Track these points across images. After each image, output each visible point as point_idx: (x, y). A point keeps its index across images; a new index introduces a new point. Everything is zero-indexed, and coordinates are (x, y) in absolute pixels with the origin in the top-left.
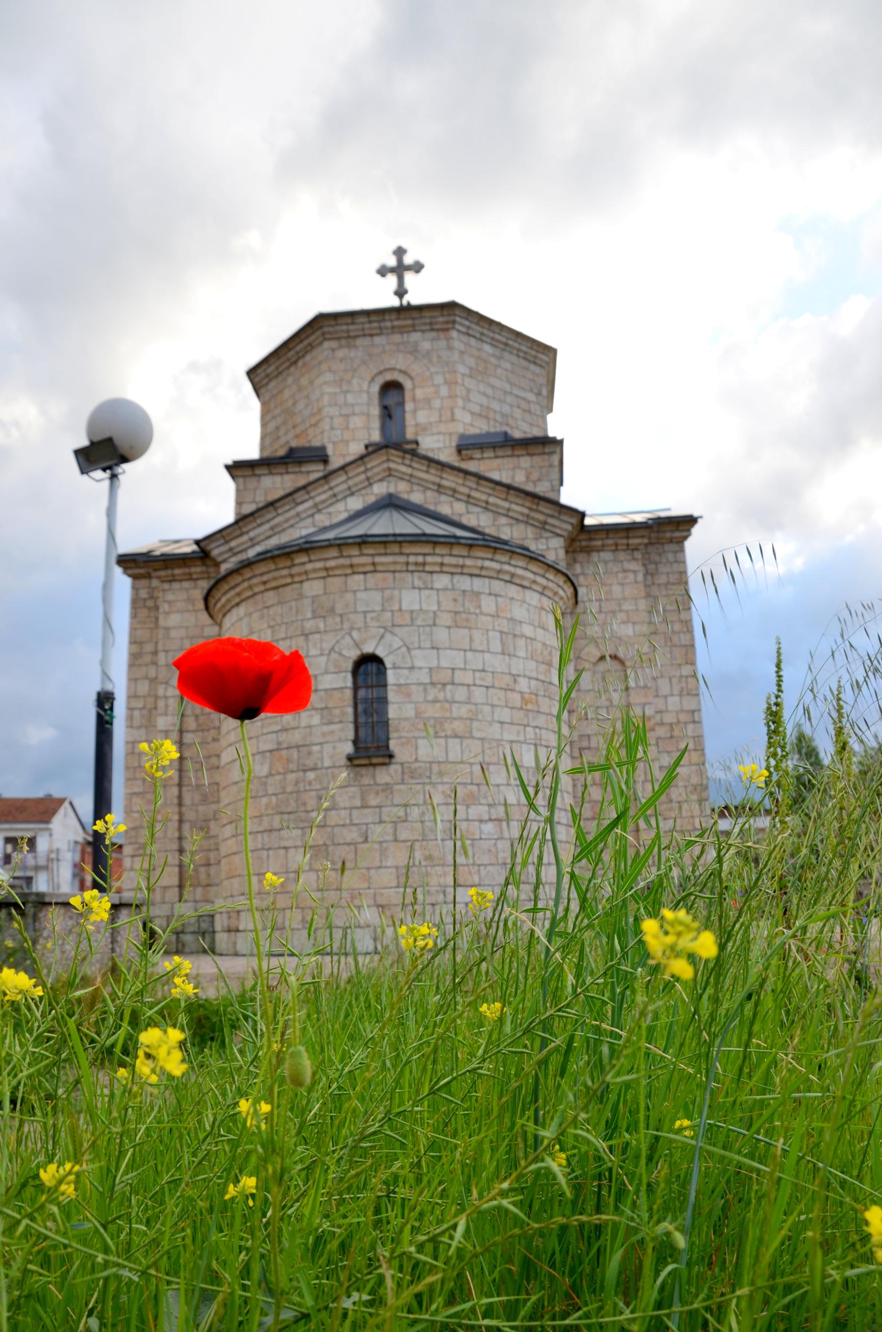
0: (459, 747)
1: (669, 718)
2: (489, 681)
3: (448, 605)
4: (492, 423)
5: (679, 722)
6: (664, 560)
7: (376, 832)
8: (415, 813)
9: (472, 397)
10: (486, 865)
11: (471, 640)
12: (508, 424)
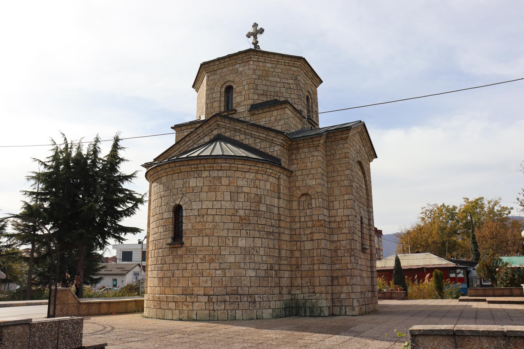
0: (208, 240)
1: (338, 219)
2: (223, 212)
3: (207, 183)
4: (269, 97)
5: (342, 221)
6: (338, 148)
7: (177, 273)
8: (189, 266)
9: (259, 88)
10: (217, 287)
11: (216, 196)
12: (277, 96)
